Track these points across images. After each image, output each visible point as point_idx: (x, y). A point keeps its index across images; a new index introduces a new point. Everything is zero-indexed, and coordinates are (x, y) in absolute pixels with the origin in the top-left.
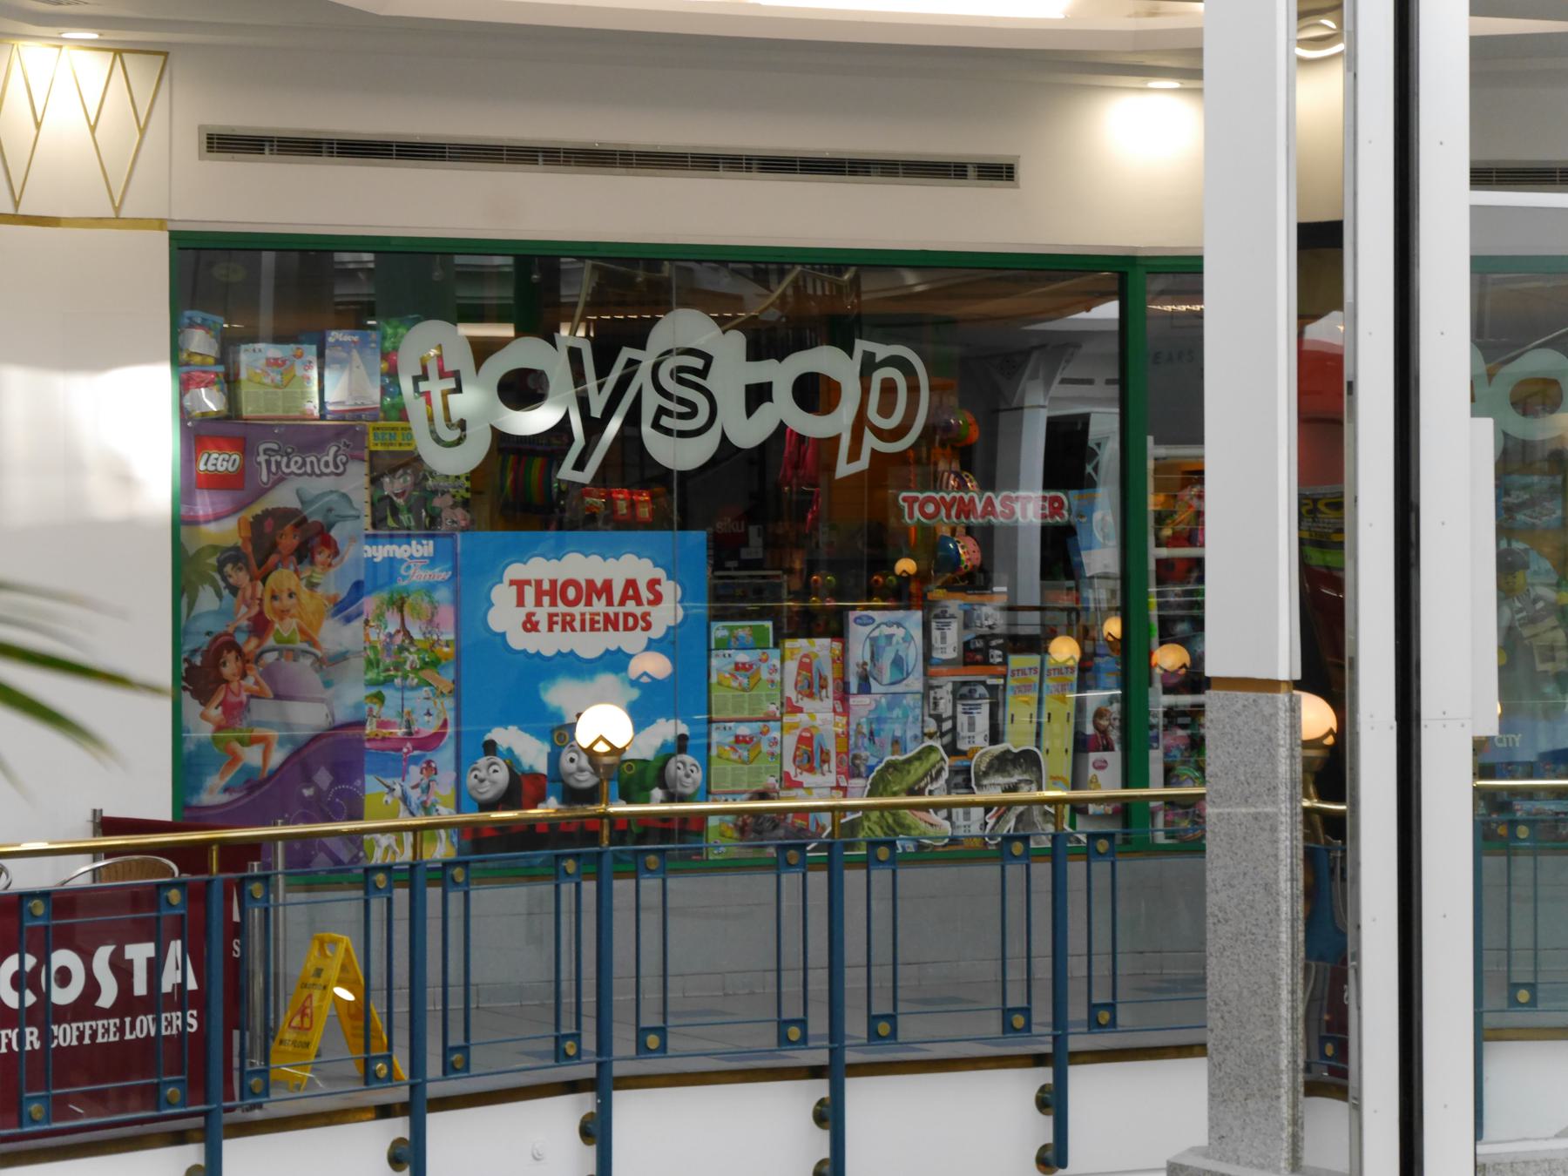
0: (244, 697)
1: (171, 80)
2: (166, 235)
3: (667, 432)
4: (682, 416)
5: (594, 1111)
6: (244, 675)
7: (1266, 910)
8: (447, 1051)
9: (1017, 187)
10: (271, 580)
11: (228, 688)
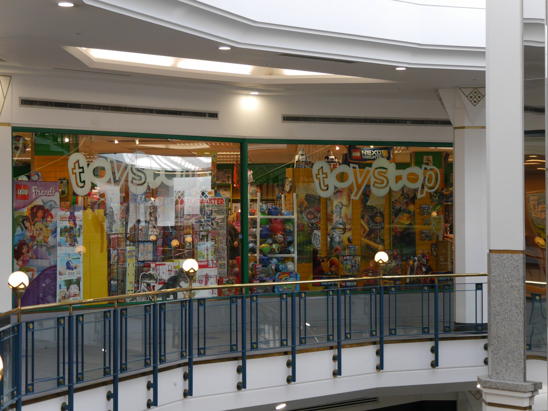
0: (28, 258)
1: (12, 84)
2: (11, 127)
3: (376, 187)
4: (380, 183)
5: (434, 345)
6: (28, 252)
7: (516, 312)
8: (252, 343)
9: (19, 97)
10: (36, 225)
11: (24, 256)
